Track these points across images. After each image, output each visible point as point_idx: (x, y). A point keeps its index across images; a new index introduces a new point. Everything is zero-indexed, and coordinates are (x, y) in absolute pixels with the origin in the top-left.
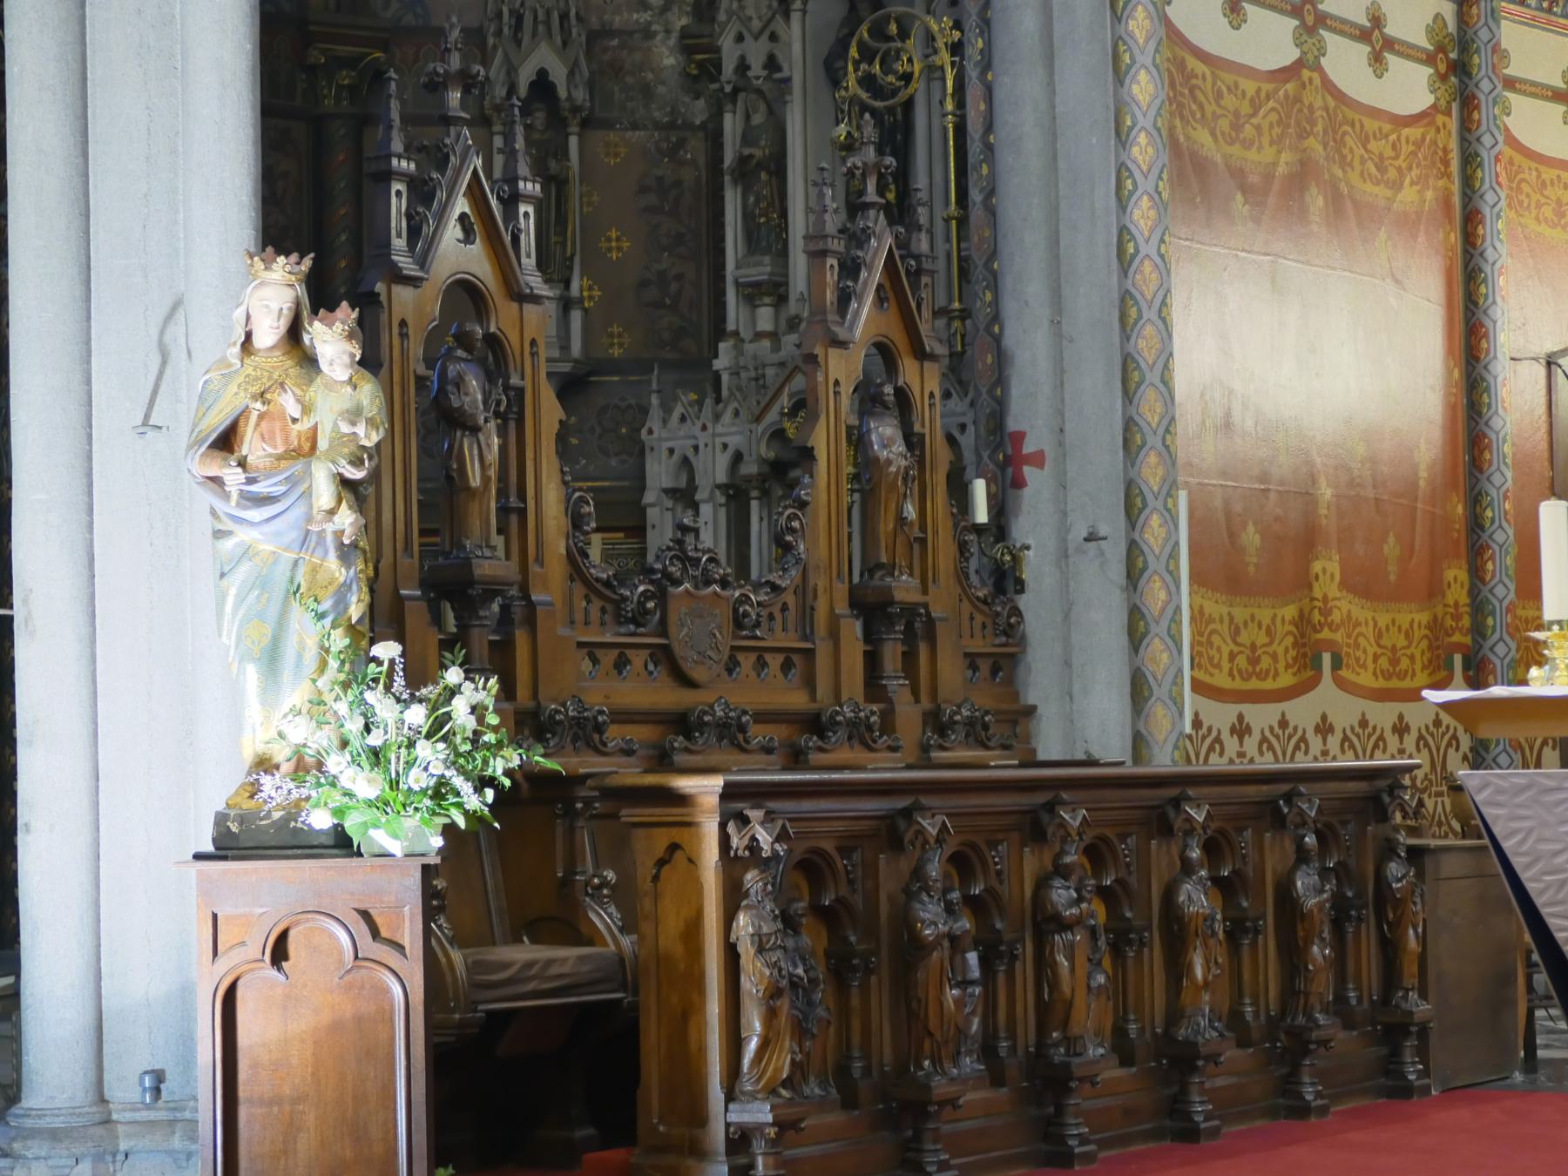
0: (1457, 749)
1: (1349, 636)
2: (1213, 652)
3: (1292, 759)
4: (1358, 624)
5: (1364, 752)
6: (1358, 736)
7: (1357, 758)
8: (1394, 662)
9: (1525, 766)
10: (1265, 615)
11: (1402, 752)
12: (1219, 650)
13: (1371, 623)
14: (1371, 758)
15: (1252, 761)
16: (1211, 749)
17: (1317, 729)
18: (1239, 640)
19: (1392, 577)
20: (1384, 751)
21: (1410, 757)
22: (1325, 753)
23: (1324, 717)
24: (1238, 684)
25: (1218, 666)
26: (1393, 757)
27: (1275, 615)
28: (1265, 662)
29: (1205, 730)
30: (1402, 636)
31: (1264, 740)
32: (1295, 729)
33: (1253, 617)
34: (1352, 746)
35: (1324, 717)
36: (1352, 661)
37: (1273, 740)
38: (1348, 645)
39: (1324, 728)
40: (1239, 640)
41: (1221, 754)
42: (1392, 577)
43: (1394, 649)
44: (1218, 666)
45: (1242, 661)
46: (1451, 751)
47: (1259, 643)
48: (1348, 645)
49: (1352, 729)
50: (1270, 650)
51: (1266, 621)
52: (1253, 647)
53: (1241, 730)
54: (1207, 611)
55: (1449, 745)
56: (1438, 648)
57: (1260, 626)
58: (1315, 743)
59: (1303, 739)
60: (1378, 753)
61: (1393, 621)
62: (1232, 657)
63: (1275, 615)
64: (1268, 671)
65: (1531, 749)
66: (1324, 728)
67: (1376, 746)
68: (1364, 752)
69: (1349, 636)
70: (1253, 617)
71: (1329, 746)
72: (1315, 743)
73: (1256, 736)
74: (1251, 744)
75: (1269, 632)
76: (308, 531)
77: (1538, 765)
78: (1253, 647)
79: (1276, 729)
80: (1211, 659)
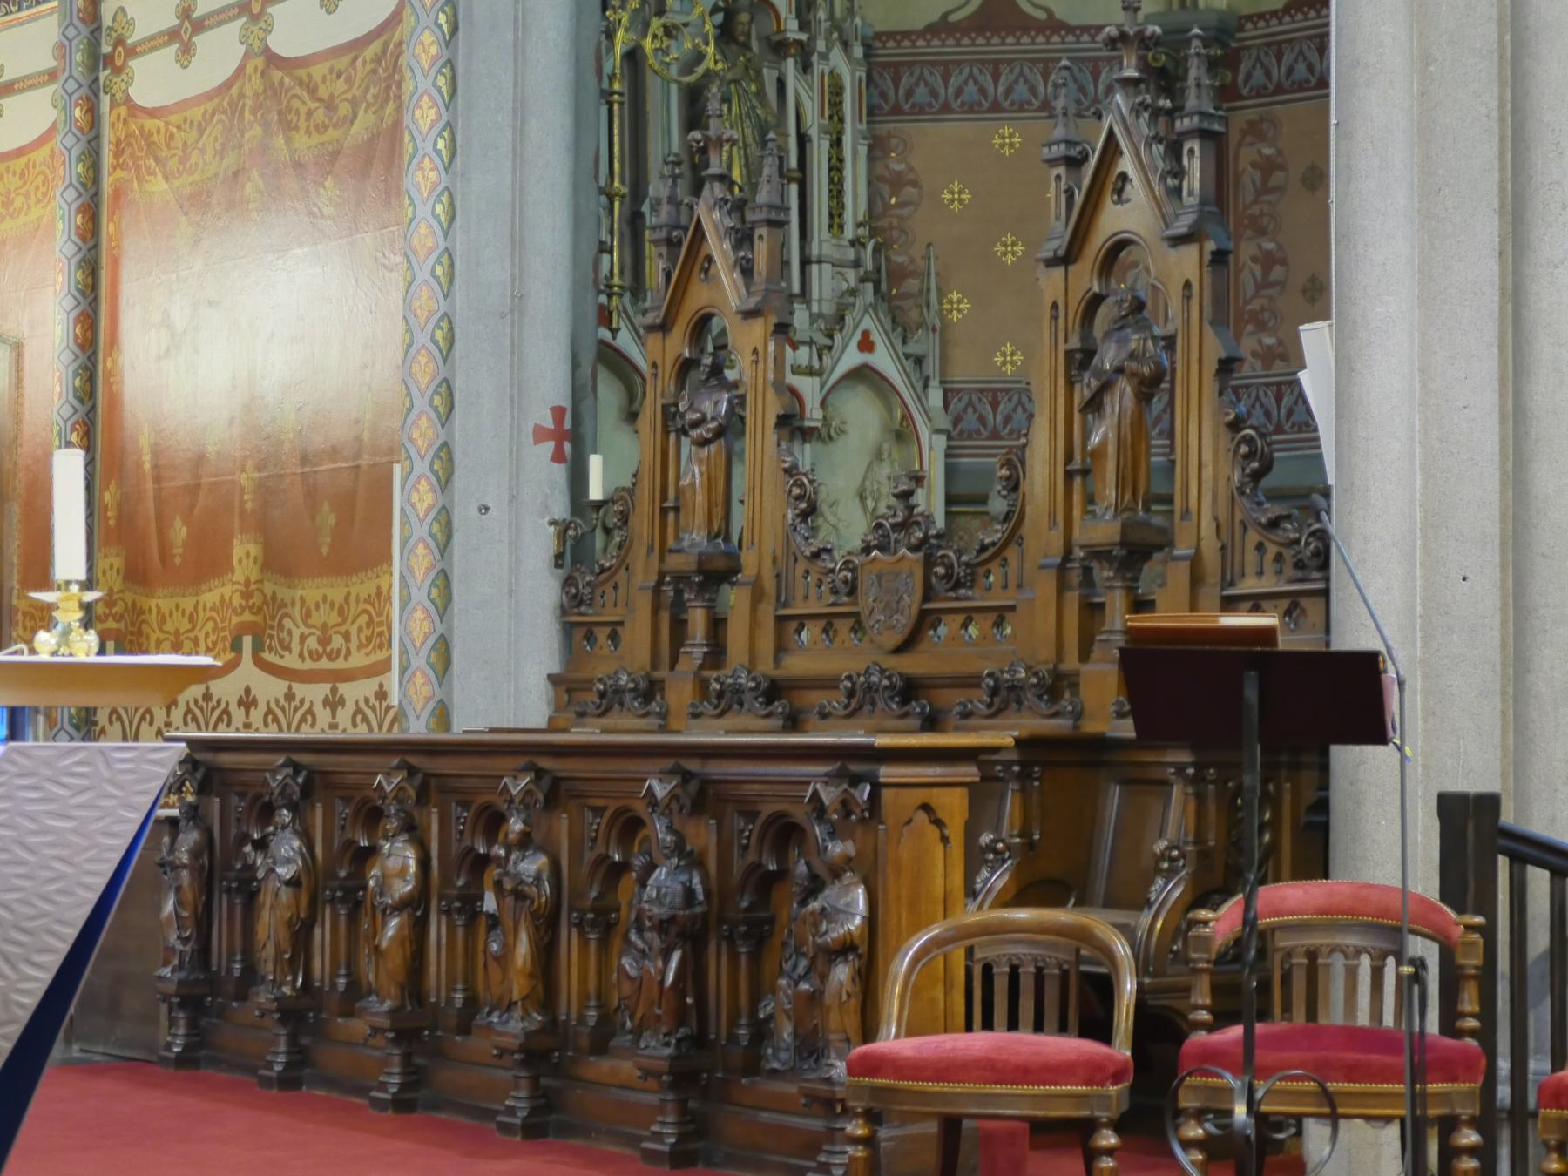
0: (151, 723)
1: (272, 618)
2: (285, 635)
3: (298, 730)
4: (284, 605)
5: (207, 725)
6: (283, 709)
7: (199, 729)
8: (324, 641)
9: (125, 739)
10: (337, 595)
11: (247, 726)
12: (290, 632)
13: (298, 604)
14: (215, 729)
15: (344, 731)
16: (303, 720)
17: (240, 703)
18: (310, 622)
19: (325, 550)
20: (229, 725)
21: (257, 730)
22: (247, 726)
23: (248, 690)
24: (309, 665)
25: (288, 648)
26: (238, 730)
27: (349, 594)
28: (337, 641)
29: (297, 702)
30: (186, 619)
31: (269, 711)
32: (219, 702)
33: (325, 598)
34: (195, 719)
35: (248, 690)
36: (275, 643)
37: (369, 712)
38: (132, 633)
39: (247, 702)
40: (310, 622)
41: (313, 725)
42: (325, 550)
43: (324, 628)
44: (288, 648)
45: (312, 643)
46: (144, 726)
47: (331, 623)
48: (132, 633)
49: (277, 701)
50: (192, 635)
51: (189, 608)
52: (177, 633)
53: (334, 703)
54: (279, 596)
55: (143, 718)
56: (224, 629)
57: (332, 605)
58: (238, 715)
59: (226, 711)
60: (221, 726)
61: (177, 607)
62: (303, 638)
63: (349, 594)
64: (339, 651)
65: (131, 724)
66: (247, 702)
67: (220, 719)
68: (207, 725)
69: (133, 624)
70: (325, 598)
71: (251, 719)
72: (238, 715)
73: (262, 708)
74: (344, 715)
75: (341, 612)
76: (1307, 496)
77: (136, 739)
78: (177, 633)
79: (282, 701)
80: (281, 642)
